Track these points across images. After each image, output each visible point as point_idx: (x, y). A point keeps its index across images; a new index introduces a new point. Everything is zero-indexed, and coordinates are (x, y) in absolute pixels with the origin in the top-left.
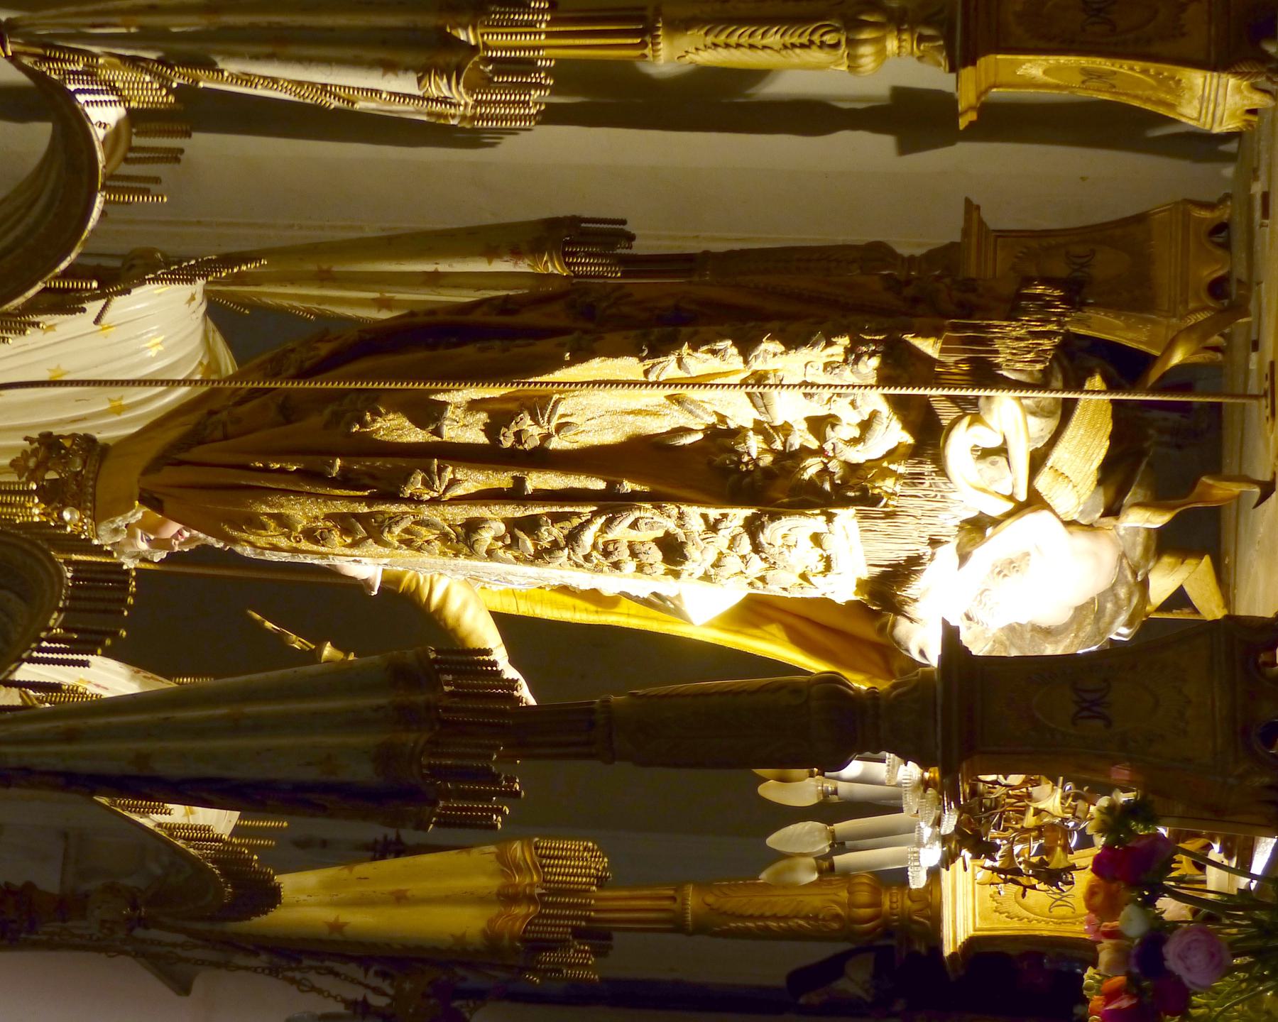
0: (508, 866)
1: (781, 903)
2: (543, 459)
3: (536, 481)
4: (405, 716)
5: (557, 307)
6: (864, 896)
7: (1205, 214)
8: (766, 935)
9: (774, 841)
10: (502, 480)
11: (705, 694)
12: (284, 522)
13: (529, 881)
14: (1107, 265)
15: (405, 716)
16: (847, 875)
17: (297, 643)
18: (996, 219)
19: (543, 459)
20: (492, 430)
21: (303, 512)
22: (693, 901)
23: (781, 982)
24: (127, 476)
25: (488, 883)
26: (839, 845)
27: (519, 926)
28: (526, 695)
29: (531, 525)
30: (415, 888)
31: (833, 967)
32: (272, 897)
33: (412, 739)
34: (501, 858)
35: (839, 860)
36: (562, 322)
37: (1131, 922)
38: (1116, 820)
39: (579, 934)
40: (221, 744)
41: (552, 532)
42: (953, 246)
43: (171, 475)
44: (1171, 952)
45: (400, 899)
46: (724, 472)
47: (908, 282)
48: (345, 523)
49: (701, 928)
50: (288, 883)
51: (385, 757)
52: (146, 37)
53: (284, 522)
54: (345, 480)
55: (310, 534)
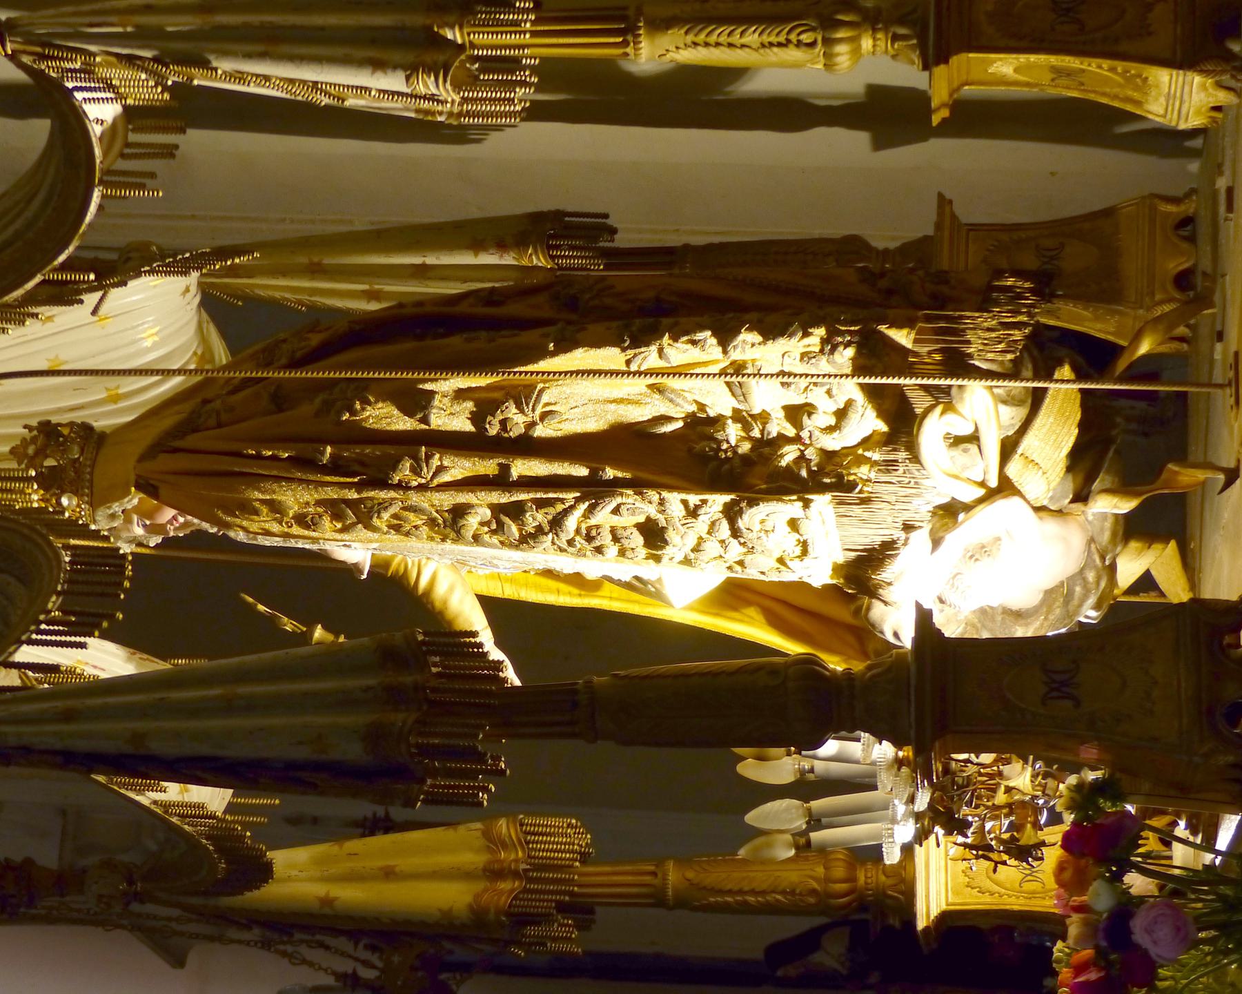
0: (494, 842)
1: (759, 878)
2: (528, 446)
3: (521, 468)
4: (394, 696)
5: (541, 299)
6: (839, 871)
7: (1171, 208)
8: (745, 909)
9: (752, 818)
10: (488, 467)
11: (685, 675)
12: (276, 508)
13: (514, 857)
14: (1075, 258)
15: (394, 696)
16: (823, 851)
17: (289, 625)
18: (968, 213)
19: (528, 446)
20: (478, 418)
21: (294, 498)
22: (674, 876)
23: (759, 955)
24: (123, 463)
25: (474, 859)
26: (816, 822)
27: (504, 901)
28: (511, 676)
29: (516, 511)
30: (403, 864)
31: (810, 941)
32: (264, 872)
33: (400, 718)
34: (487, 834)
35: (815, 836)
36: (546, 313)
37: (1099, 897)
38: (1085, 798)
39: (562, 908)
40: (214, 724)
41: (536, 517)
42: (926, 239)
43: (166, 462)
44: (1138, 926)
45: (389, 874)
46: (704, 459)
47: (882, 275)
48: (336, 509)
49: (682, 903)
50: (280, 858)
51: (374, 736)
52: (142, 36)
53: (276, 508)
54: (336, 467)
55: (301, 520)
